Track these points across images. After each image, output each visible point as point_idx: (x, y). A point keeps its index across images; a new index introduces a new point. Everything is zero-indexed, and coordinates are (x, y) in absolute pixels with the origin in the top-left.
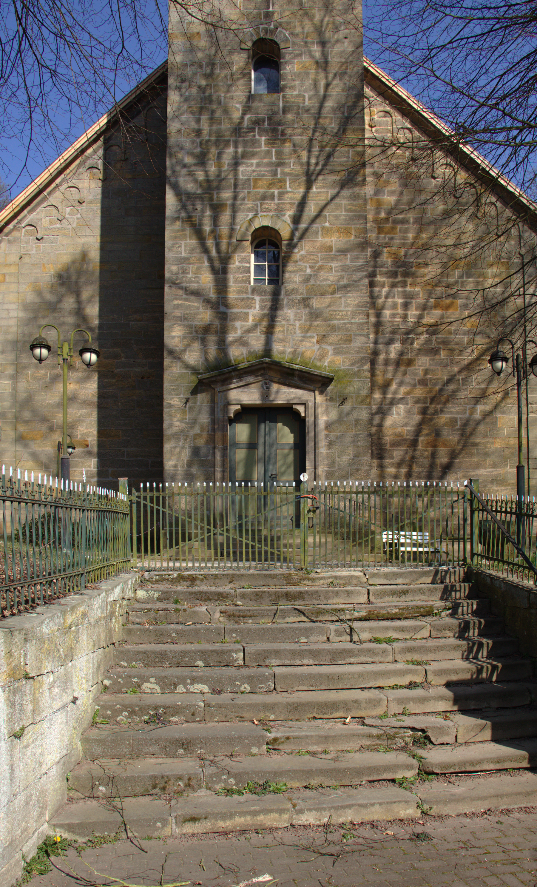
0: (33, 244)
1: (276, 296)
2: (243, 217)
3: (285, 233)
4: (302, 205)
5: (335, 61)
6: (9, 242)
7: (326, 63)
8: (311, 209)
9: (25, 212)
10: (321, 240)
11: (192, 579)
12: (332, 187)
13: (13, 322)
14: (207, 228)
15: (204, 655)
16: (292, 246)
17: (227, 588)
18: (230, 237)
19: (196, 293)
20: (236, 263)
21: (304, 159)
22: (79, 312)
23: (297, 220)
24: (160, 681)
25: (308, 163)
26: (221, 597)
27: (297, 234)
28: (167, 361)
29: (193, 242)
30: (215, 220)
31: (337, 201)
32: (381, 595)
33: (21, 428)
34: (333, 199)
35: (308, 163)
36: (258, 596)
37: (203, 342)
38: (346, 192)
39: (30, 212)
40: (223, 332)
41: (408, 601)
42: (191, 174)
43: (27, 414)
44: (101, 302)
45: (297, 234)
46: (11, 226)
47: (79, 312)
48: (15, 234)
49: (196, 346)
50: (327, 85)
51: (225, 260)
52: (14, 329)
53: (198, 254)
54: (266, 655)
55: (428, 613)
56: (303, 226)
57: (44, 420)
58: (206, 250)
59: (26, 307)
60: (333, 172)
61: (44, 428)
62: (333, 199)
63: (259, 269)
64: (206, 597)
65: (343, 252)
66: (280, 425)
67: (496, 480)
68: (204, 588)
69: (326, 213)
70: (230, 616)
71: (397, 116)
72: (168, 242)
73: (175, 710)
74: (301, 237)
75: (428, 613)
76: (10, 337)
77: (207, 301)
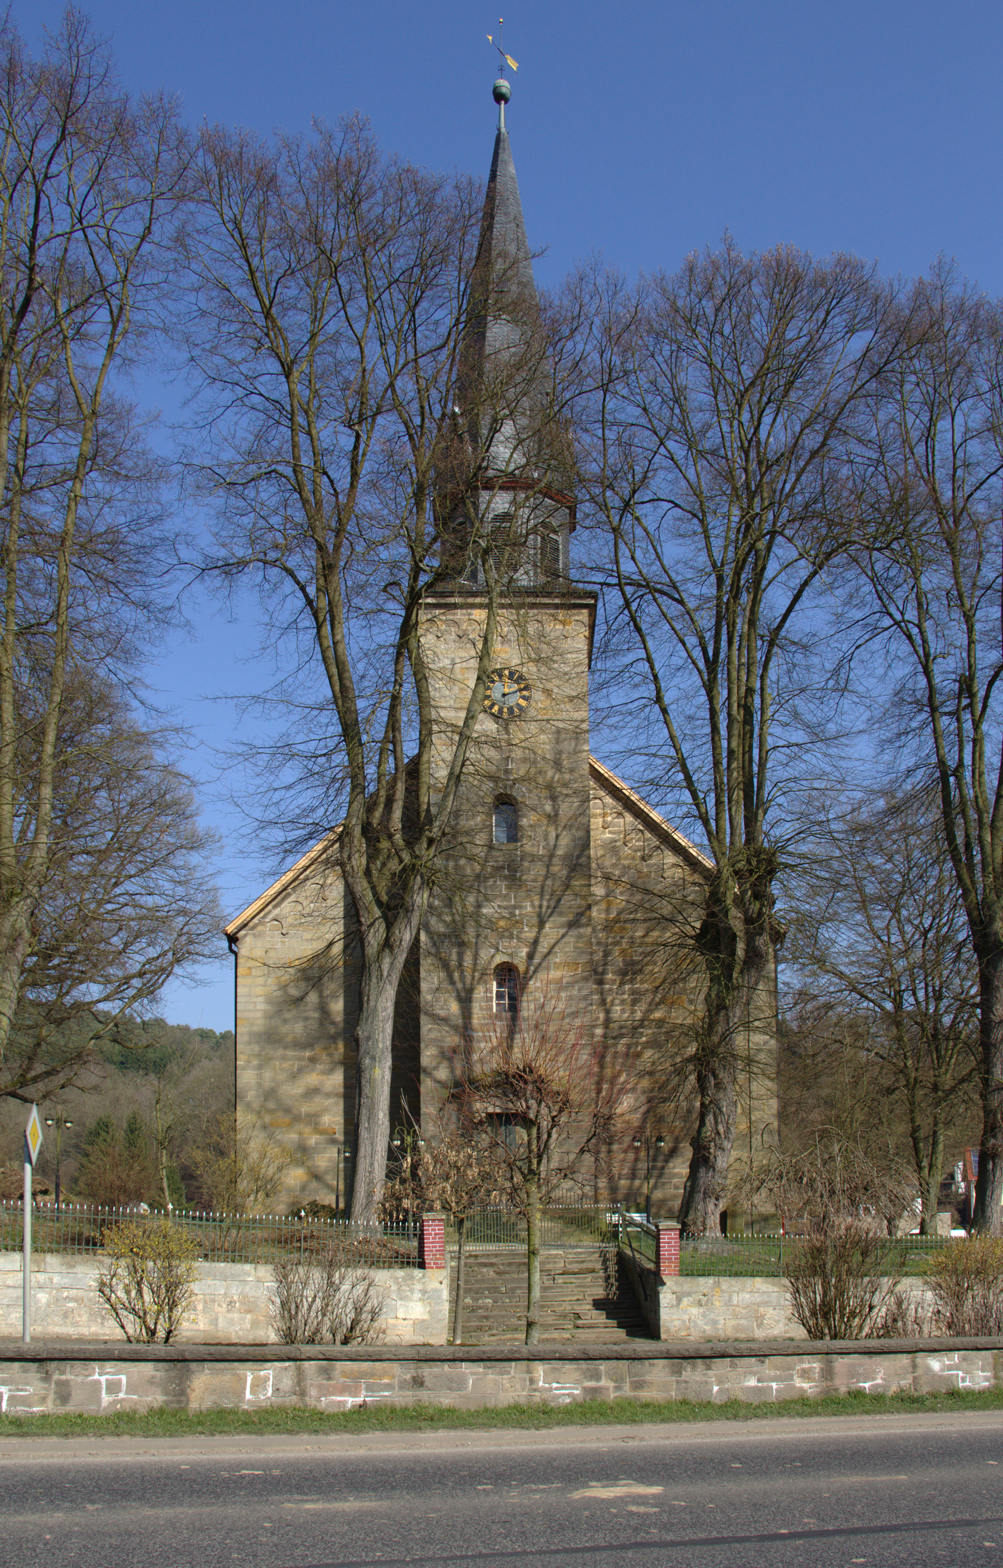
0: (279, 938)
1: (514, 1019)
2: (485, 954)
3: (522, 968)
4: (536, 942)
5: (563, 819)
6: (254, 936)
7: (556, 815)
8: (543, 948)
9: (270, 907)
10: (554, 974)
11: (476, 1256)
12: (562, 926)
13: (259, 1014)
14: (454, 963)
15: (488, 1289)
16: (527, 977)
17: (494, 1260)
18: (474, 970)
19: (445, 1020)
20: (479, 993)
21: (537, 903)
22: (323, 1009)
23: (531, 956)
24: (472, 1298)
25: (541, 906)
26: (492, 1265)
27: (532, 968)
28: (422, 1076)
29: (443, 975)
30: (461, 956)
31: (566, 939)
32: (571, 1263)
33: (267, 1119)
34: (563, 936)
35: (541, 906)
36: (510, 1264)
37: (450, 1060)
38: (574, 932)
39: (275, 907)
40: (468, 1051)
41: (584, 1266)
42: (439, 916)
43: (271, 1105)
44: (345, 997)
45: (532, 968)
46: (256, 920)
47: (323, 1009)
48: (260, 928)
49: (445, 1064)
50: (557, 836)
51: (470, 991)
52: (260, 1022)
53: (445, 985)
54: (515, 1288)
55: (593, 1271)
56: (536, 961)
57: (287, 1111)
58: (452, 982)
59: (269, 1001)
60: (561, 914)
61: (287, 1119)
62: (563, 936)
63: (500, 996)
64: (485, 1265)
65: (571, 985)
66: (518, 1128)
67: (571, 1222)
68: (483, 1260)
69: (556, 949)
70: (498, 1273)
71: (629, 818)
72: (423, 974)
73: (480, 1308)
74: (535, 972)
75: (593, 1271)
76: (256, 1029)
77: (455, 1028)
